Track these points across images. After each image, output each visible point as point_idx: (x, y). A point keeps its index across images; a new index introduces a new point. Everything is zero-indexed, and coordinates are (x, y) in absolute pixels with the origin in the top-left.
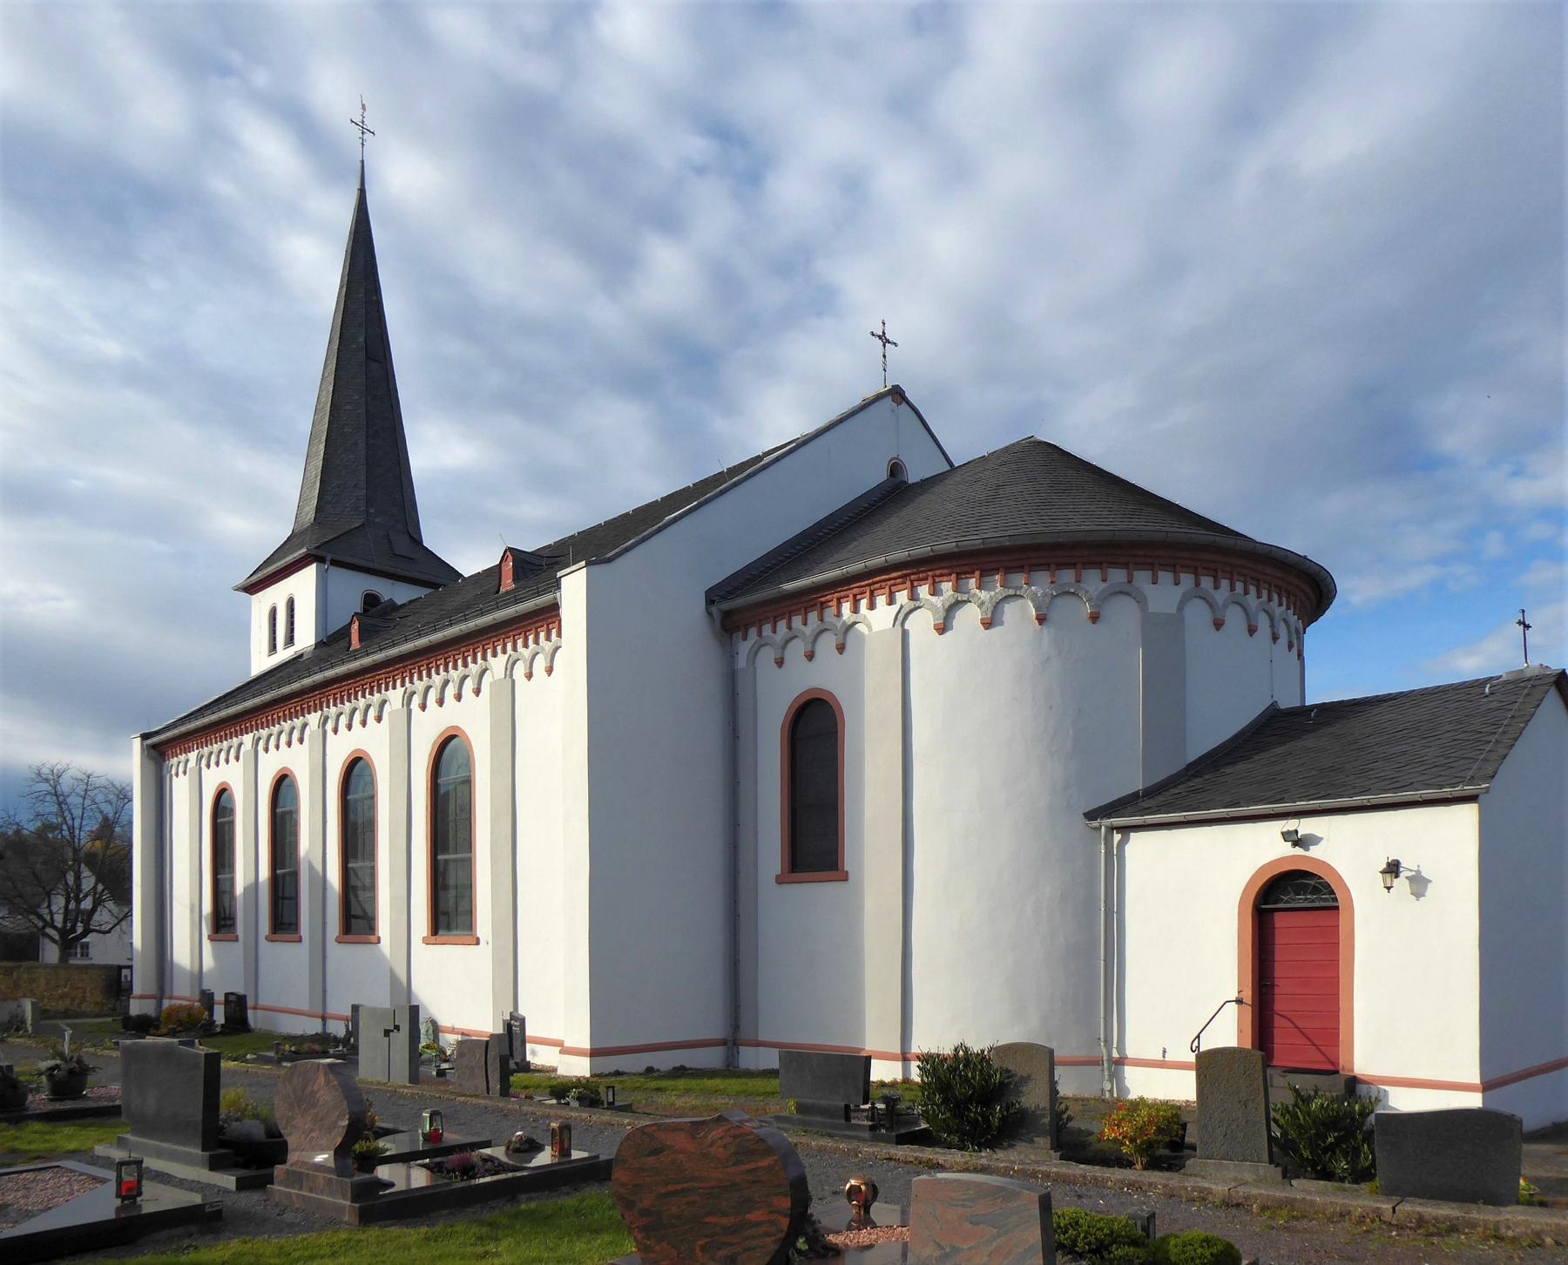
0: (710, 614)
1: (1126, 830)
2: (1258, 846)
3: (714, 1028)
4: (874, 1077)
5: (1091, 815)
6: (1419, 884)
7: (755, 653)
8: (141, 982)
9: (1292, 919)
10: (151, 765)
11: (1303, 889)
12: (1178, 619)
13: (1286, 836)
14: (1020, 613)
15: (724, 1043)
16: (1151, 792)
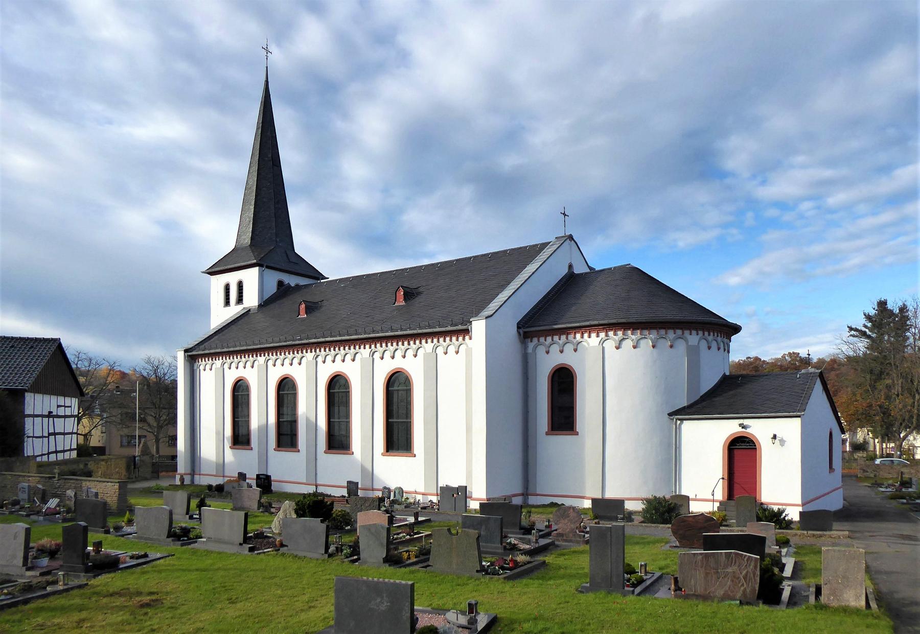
0: (519, 333)
1: (682, 420)
2: (729, 428)
3: (519, 489)
5: (670, 414)
6: (782, 442)
7: (535, 347)
8: (182, 465)
9: (741, 452)
10: (188, 364)
11: (744, 442)
12: (698, 347)
13: (740, 425)
14: (647, 344)
15: (523, 495)
16: (689, 406)
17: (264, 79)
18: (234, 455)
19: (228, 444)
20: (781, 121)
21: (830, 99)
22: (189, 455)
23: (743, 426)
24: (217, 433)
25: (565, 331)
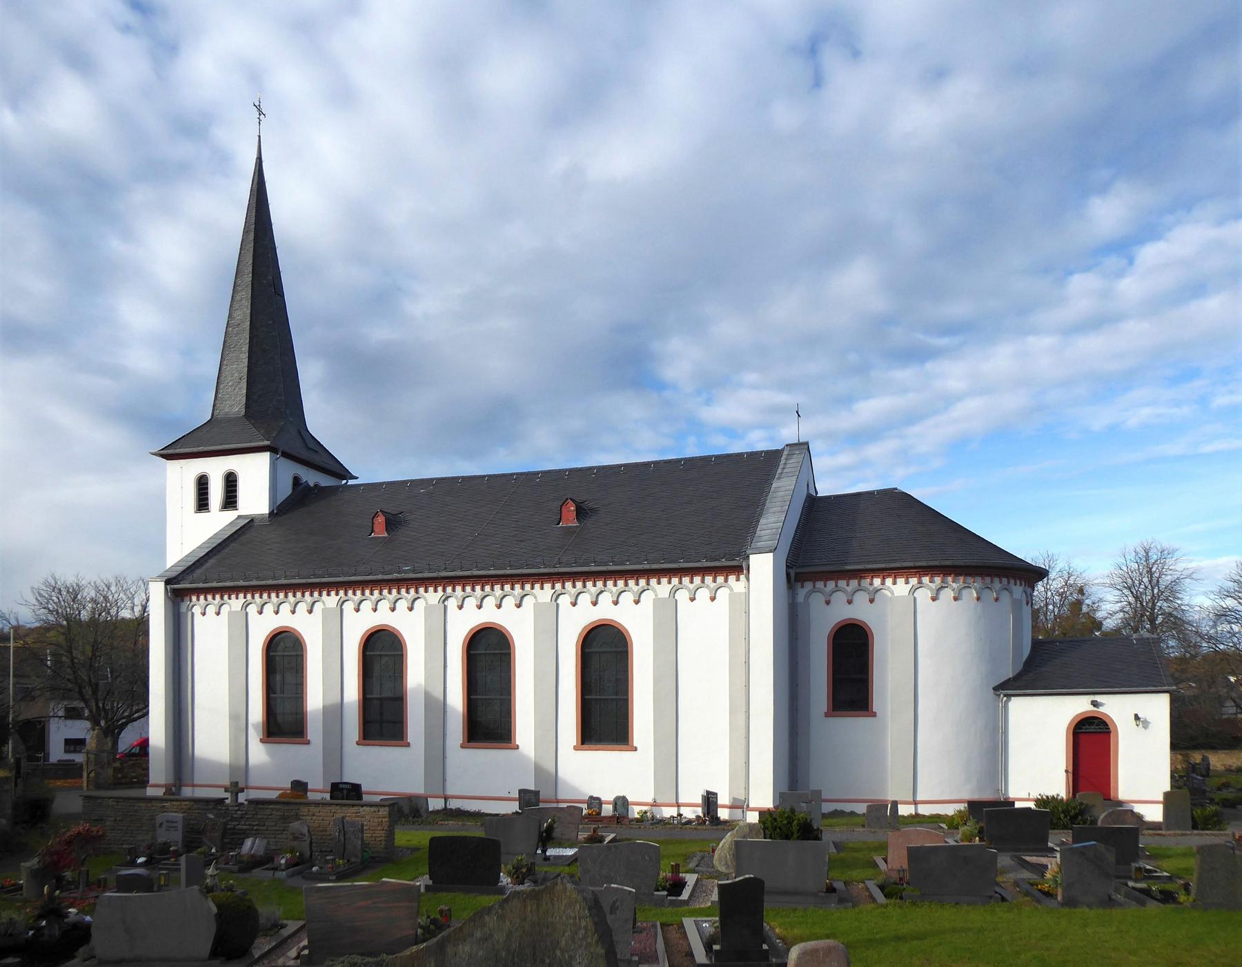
1: (1009, 696)
2: (1079, 705)
4: (900, 813)
5: (996, 689)
6: (1146, 724)
8: (159, 771)
9: (1091, 739)
11: (1091, 724)
17: (255, 156)
18: (269, 753)
19: (255, 737)
20: (730, 329)
21: (786, 308)
22: (171, 753)
23: (1095, 704)
24: (233, 717)
25: (858, 574)
